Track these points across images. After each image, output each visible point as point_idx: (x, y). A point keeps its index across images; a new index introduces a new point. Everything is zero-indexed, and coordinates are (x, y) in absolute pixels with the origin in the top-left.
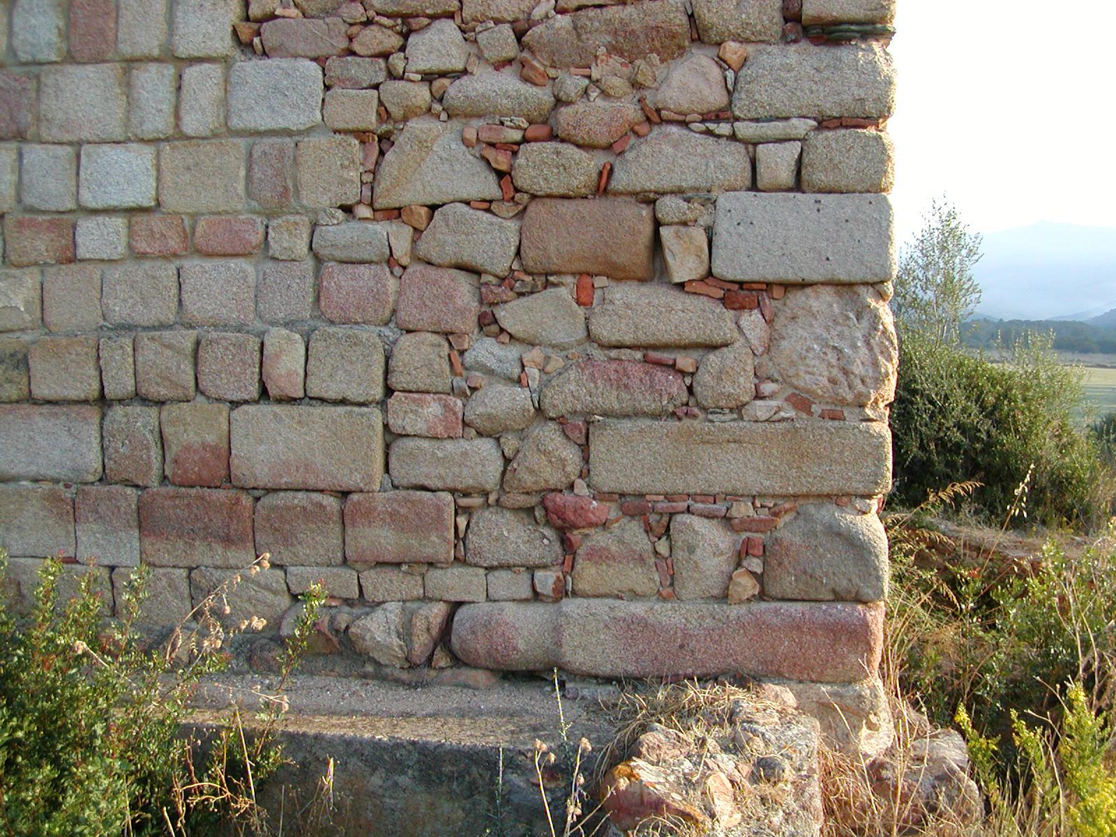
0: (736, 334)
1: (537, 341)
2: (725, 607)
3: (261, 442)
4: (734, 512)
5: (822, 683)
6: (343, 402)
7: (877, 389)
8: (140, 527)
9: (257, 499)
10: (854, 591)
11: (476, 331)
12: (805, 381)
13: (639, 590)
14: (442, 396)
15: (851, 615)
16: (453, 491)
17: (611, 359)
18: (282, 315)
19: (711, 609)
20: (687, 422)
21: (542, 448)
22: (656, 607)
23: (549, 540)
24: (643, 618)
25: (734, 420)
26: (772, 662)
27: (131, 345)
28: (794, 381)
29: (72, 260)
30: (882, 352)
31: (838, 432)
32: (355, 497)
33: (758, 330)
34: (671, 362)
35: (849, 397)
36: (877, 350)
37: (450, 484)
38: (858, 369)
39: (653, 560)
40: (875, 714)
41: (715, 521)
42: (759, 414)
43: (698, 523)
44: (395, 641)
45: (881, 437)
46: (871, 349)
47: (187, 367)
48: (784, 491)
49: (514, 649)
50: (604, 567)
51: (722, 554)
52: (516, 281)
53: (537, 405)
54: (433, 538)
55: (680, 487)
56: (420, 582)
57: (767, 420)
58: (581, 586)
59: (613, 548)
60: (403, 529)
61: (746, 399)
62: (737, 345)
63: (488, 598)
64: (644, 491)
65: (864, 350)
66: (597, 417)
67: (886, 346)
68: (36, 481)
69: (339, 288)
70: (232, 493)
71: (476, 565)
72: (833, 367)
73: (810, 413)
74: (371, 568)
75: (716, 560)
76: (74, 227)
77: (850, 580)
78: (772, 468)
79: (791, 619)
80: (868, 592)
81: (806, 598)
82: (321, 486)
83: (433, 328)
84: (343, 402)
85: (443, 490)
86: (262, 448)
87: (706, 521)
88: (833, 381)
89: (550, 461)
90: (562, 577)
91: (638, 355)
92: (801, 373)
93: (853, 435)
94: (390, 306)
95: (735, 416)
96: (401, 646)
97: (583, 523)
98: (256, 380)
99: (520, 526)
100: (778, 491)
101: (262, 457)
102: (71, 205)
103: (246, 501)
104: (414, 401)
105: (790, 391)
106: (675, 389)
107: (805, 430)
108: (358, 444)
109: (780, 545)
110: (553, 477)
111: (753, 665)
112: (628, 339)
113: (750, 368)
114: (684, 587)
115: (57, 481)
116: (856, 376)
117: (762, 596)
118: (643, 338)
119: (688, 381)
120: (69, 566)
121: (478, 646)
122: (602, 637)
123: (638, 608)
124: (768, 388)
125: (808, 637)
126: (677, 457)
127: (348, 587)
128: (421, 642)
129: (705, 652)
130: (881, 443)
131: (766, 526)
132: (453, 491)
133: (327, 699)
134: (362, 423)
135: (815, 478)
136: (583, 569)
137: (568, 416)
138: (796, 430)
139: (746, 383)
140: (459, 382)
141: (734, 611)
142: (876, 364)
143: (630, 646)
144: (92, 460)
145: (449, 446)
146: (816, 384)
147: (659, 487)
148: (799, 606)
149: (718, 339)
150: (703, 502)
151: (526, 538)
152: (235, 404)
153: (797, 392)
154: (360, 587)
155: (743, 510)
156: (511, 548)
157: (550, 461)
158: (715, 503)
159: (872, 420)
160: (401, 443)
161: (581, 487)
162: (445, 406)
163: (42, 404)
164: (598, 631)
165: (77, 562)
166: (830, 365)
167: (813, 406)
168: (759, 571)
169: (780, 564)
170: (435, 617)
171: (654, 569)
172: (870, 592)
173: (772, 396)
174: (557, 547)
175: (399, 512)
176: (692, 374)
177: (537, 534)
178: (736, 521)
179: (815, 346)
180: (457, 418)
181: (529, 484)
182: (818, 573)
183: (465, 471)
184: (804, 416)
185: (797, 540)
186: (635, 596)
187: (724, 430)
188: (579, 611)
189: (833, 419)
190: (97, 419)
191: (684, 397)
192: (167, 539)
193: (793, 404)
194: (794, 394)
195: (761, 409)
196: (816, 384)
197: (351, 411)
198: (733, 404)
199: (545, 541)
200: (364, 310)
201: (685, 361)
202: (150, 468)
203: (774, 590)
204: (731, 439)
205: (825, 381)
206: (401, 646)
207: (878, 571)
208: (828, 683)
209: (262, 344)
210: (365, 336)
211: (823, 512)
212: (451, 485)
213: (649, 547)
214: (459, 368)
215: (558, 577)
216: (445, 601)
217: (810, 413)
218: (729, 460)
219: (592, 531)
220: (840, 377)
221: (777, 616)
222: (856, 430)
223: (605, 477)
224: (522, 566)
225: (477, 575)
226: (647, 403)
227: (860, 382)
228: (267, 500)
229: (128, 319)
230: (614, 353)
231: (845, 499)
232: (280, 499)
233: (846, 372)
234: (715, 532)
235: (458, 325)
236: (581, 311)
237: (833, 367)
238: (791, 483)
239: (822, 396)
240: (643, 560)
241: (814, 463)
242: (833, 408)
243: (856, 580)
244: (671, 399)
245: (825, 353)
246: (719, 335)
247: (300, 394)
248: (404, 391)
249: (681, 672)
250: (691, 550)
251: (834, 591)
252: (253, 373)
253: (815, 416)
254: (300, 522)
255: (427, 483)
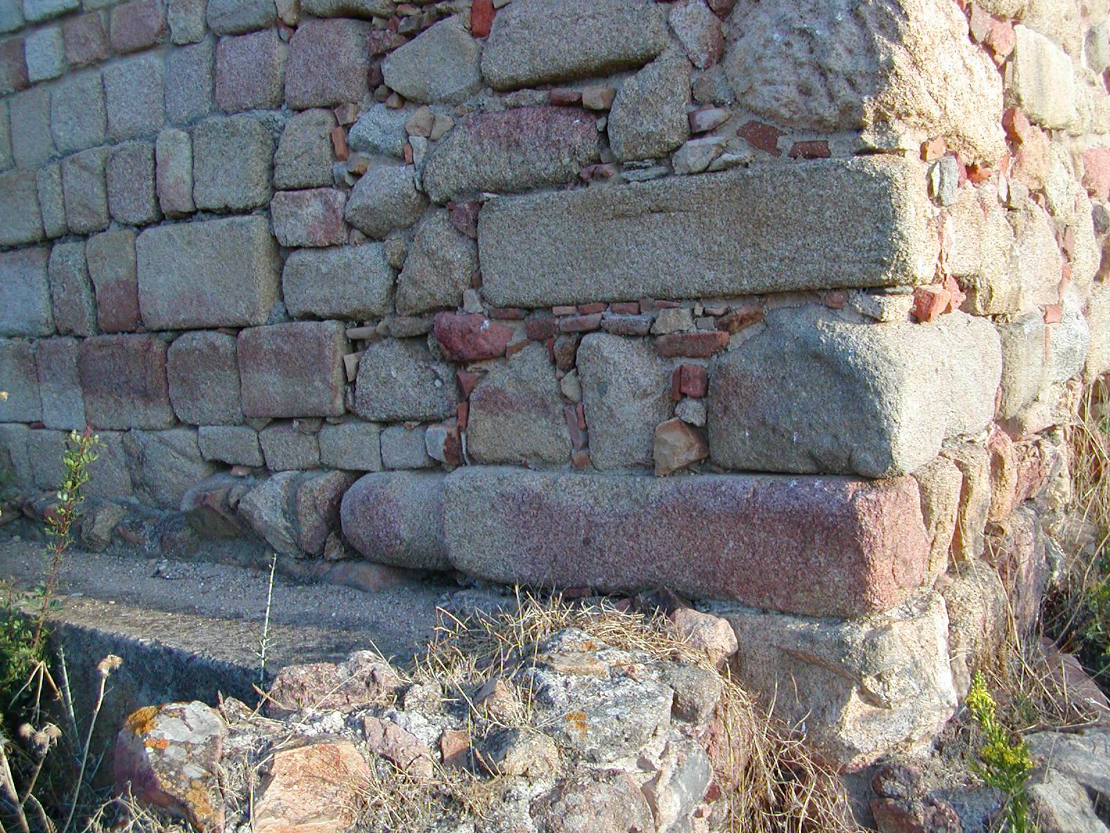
0: (664, 38)
1: (429, 99)
2: (648, 480)
3: (159, 272)
4: (659, 328)
5: (795, 615)
6: (227, 212)
7: (876, 94)
8: (82, 383)
9: (169, 343)
10: (843, 456)
11: (366, 97)
12: (763, 97)
13: (545, 453)
14: (323, 190)
15: (828, 498)
16: (343, 319)
17: (509, 108)
18: (185, 113)
19: (630, 483)
20: (595, 186)
21: (425, 248)
22: (562, 480)
23: (442, 380)
24: (538, 495)
25: (663, 176)
26: (714, 574)
27: (57, 172)
28: (750, 100)
29: (27, 85)
30: (881, 27)
31: (811, 177)
32: (244, 333)
33: (697, 28)
34: (575, 99)
35: (830, 113)
36: (872, 24)
37: (336, 308)
38: (839, 61)
39: (560, 406)
40: (879, 678)
41: (637, 343)
42: (691, 160)
43: (607, 345)
44: (281, 522)
45: (887, 178)
46: (861, 23)
47: (98, 190)
48: (734, 287)
49: (397, 537)
50: (501, 419)
51: (645, 395)
52: (401, 18)
53: (419, 187)
54: (317, 383)
55: (592, 292)
56: (314, 444)
57: (705, 171)
58: (478, 447)
59: (510, 390)
60: (288, 372)
61: (674, 139)
62: (666, 55)
63: (385, 468)
64: (549, 300)
65: (849, 28)
66: (487, 195)
67: (888, 16)
68: (10, 337)
69: (231, 67)
70: (144, 338)
71: (365, 420)
72: (801, 65)
73: (777, 152)
74: (268, 425)
75: (638, 404)
76: (23, 46)
77: (835, 437)
78: (716, 248)
79: (734, 503)
80: (866, 459)
81: (768, 467)
82: (213, 321)
83: (320, 102)
84: (227, 212)
85: (330, 318)
86: (161, 279)
87: (622, 341)
88: (806, 91)
89: (435, 267)
90: (455, 434)
91: (540, 95)
92: (757, 85)
93: (838, 178)
94: (278, 81)
95: (663, 170)
96: (286, 528)
97: (473, 355)
98: (151, 196)
99: (412, 362)
100: (727, 286)
101: (162, 291)
102: (18, 22)
103: (158, 345)
104: (293, 199)
105: (746, 119)
106: (578, 139)
107: (760, 178)
108: (239, 262)
109: (725, 377)
110: (441, 291)
111: (686, 579)
112: (523, 73)
113: (681, 90)
114: (599, 449)
115: (22, 336)
116: (837, 73)
117: (706, 463)
118: (543, 67)
119: (601, 124)
120: (37, 431)
121: (360, 531)
122: (489, 523)
123: (533, 481)
124: (708, 117)
125: (763, 535)
126: (584, 243)
127: (248, 452)
128: (310, 522)
129: (618, 553)
130: (885, 188)
131: (708, 347)
132: (343, 319)
133: (188, 593)
134: (242, 235)
135: (781, 260)
136: (475, 421)
137: (455, 198)
138: (747, 180)
139: (673, 114)
140: (341, 169)
141: (658, 487)
142: (871, 50)
143: (524, 538)
144: (42, 308)
145: (333, 256)
146: (777, 100)
147: (564, 293)
148: (752, 481)
149: (636, 51)
150: (621, 312)
151: (416, 380)
152: (141, 227)
153: (758, 119)
154: (262, 452)
155: (676, 321)
156: (399, 392)
157: (435, 267)
158: (640, 313)
159: (871, 151)
160: (295, 258)
161: (473, 303)
162: (326, 203)
163: (7, 251)
164: (483, 514)
165: (43, 427)
166: (798, 64)
167: (780, 139)
168: (698, 421)
169: (726, 409)
170: (322, 491)
171: (562, 420)
172: (870, 458)
173: (712, 131)
174: (451, 392)
175: (283, 349)
176: (606, 112)
177: (429, 372)
178: (662, 339)
179: (776, 36)
180: (337, 217)
181: (414, 302)
182: (784, 424)
183: (350, 289)
184: (767, 157)
185: (756, 369)
186: (545, 463)
187: (642, 193)
188: (462, 483)
189: (812, 157)
190: (42, 263)
191: (591, 150)
192: (101, 397)
193: (749, 139)
194: (752, 124)
195: (694, 154)
196: (777, 100)
197: (232, 222)
198: (655, 150)
199: (438, 383)
200: (253, 92)
201: (592, 94)
202: (83, 315)
203: (721, 454)
204: (654, 208)
205: (791, 92)
206: (286, 528)
207: (879, 421)
208: (804, 616)
209: (155, 150)
210: (242, 121)
211: (801, 320)
212: (336, 310)
213: (552, 386)
214: (340, 149)
215: (449, 435)
216: (341, 470)
217: (777, 152)
218: (653, 240)
219: (490, 366)
220: (816, 82)
221: (715, 496)
222: (840, 171)
223: (501, 288)
224: (416, 420)
225: (368, 433)
226: (544, 166)
227: (846, 85)
228: (179, 344)
229: (71, 145)
230: (510, 99)
231: (837, 296)
232: (196, 340)
233: (823, 72)
234: (635, 359)
235: (339, 90)
236: (472, 44)
237: (801, 65)
238: (745, 272)
239: (790, 120)
240: (546, 406)
241: (778, 234)
242: (814, 138)
243: (846, 437)
244: (574, 154)
245: (788, 44)
246: (636, 44)
247: (187, 207)
248: (286, 190)
249: (589, 583)
250: (602, 389)
251: (812, 457)
252: (148, 187)
253: (784, 155)
254: (200, 369)
255: (315, 309)
